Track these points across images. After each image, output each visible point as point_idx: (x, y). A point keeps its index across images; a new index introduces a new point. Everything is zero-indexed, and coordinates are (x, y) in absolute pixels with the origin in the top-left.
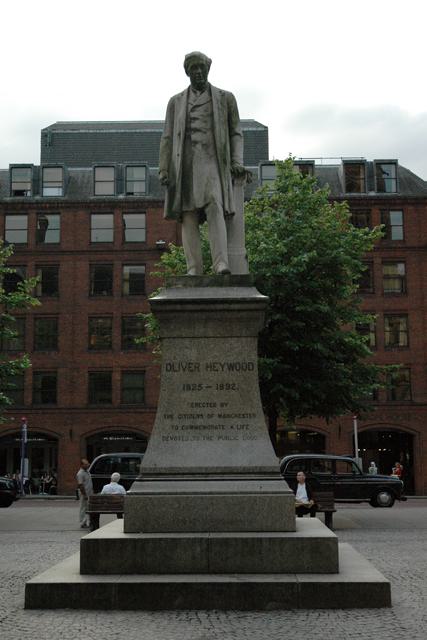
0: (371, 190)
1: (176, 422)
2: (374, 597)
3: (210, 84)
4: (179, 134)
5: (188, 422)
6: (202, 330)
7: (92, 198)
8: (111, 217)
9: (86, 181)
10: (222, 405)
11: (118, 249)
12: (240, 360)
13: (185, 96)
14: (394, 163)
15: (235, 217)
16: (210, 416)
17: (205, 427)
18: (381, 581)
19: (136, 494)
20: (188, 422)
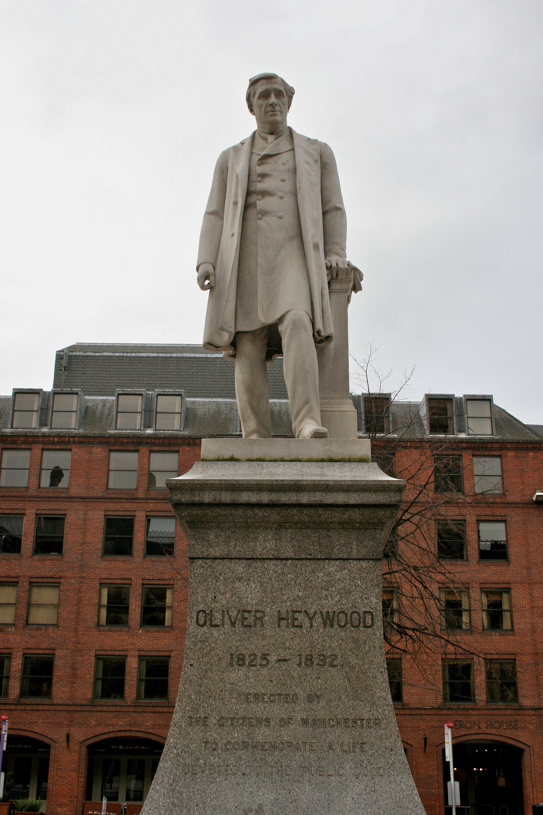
3: (290, 129)
4: (236, 203)
5: (238, 735)
6: (270, 545)
7: (112, 432)
9: (106, 412)
10: (310, 699)
11: (141, 496)
12: (347, 605)
13: (247, 147)
14: (488, 399)
16: (285, 722)
17: (273, 747)
20: (238, 735)
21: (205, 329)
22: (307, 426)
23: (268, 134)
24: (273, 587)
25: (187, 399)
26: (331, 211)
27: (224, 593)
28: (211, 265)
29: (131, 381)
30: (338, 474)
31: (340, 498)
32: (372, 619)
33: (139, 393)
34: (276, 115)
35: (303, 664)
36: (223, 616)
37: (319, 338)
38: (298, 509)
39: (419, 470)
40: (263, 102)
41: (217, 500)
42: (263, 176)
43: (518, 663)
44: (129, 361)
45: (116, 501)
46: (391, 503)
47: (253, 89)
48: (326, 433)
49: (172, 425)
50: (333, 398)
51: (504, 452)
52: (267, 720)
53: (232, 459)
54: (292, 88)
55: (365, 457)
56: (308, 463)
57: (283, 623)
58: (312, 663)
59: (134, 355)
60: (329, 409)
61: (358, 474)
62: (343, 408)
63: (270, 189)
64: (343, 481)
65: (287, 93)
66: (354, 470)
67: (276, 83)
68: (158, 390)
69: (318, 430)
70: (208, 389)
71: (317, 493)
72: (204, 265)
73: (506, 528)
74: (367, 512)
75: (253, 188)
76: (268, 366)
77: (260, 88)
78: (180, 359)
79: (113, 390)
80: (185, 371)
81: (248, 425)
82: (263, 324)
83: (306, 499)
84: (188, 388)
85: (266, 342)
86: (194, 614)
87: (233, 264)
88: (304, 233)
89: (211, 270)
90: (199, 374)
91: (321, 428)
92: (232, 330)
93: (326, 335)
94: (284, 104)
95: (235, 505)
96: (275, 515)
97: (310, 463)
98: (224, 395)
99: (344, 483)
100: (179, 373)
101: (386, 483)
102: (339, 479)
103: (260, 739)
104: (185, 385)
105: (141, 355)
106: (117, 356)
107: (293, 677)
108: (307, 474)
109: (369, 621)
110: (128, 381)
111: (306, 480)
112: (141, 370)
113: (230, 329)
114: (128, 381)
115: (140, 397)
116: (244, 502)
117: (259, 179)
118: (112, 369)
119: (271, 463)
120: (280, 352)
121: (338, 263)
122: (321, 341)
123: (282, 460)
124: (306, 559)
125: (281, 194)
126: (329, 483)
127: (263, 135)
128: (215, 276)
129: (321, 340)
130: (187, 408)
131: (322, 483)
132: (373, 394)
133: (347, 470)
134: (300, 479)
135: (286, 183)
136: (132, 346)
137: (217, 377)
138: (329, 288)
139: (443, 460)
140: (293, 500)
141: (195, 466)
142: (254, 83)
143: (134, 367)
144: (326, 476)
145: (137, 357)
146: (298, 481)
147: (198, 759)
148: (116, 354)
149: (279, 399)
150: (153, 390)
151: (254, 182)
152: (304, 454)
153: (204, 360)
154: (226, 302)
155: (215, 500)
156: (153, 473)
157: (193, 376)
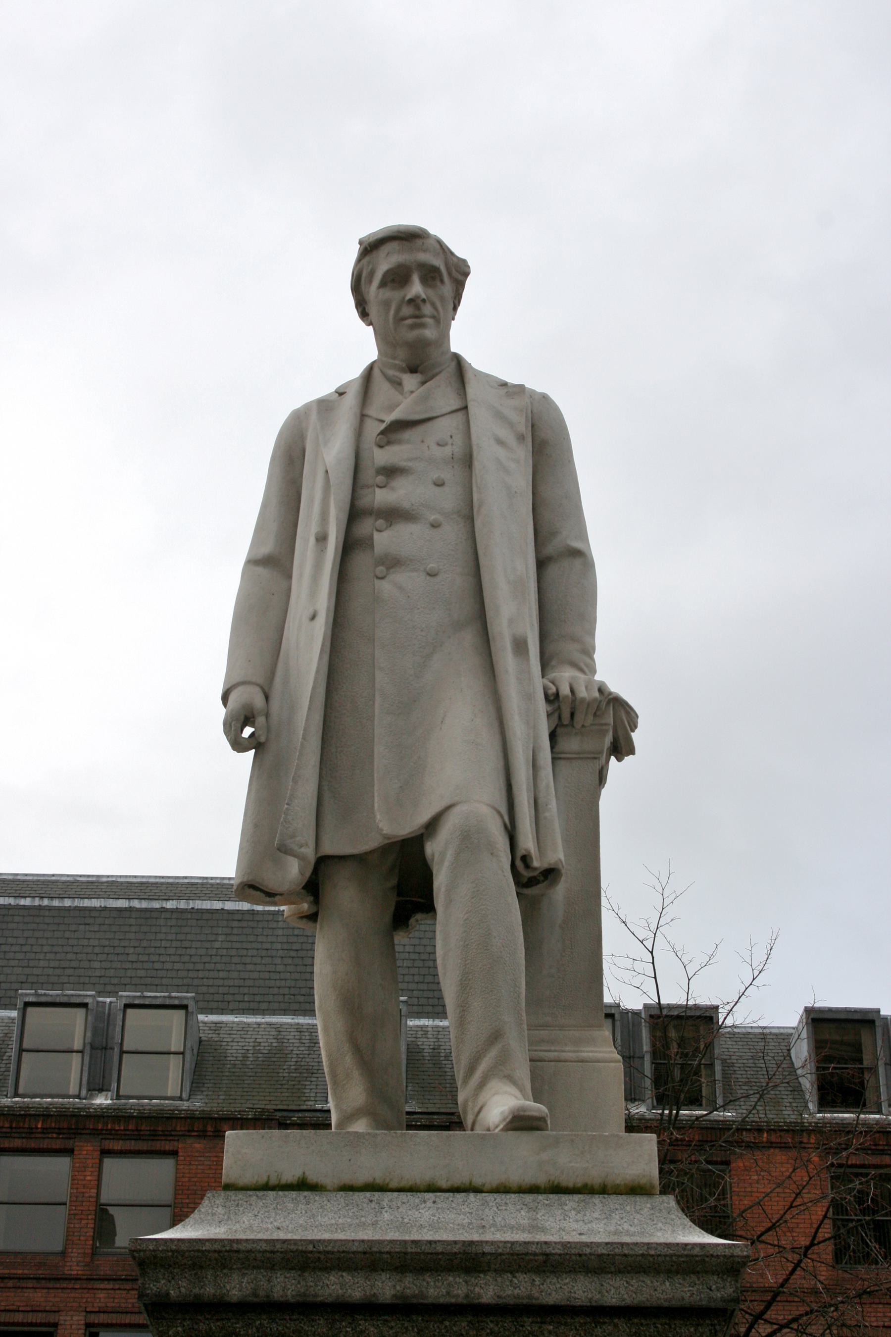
3: (458, 360)
4: (322, 539)
8: (63, 1164)
13: (351, 401)
21: (241, 849)
22: (496, 1098)
23: (403, 371)
25: (201, 1017)
26: (559, 559)
28: (257, 690)
29: (58, 972)
30: (575, 1226)
31: (581, 1290)
33: (78, 1001)
34: (423, 326)
37: (526, 874)
38: (470, 1318)
39: (791, 1207)
40: (395, 295)
41: (262, 1293)
42: (391, 472)
44: (57, 920)
45: (10, 1284)
46: (713, 1305)
47: (369, 263)
48: (542, 1119)
49: (161, 1084)
50: (562, 1027)
53: (303, 1185)
54: (464, 261)
55: (643, 1181)
56: (499, 1198)
59: (67, 903)
60: (552, 1055)
61: (626, 1226)
62: (588, 1052)
63: (406, 505)
64: (587, 1245)
65: (450, 274)
66: (616, 1217)
67: (425, 251)
68: (127, 995)
69: (523, 1109)
70: (255, 990)
71: (521, 1276)
72: (240, 689)
75: (365, 501)
76: (396, 942)
77: (385, 262)
78: (185, 916)
79: (12, 993)
80: (198, 944)
81: (344, 1097)
82: (386, 837)
83: (491, 1293)
84: (204, 989)
85: (394, 881)
87: (314, 688)
88: (489, 614)
89: (259, 701)
90: (233, 952)
91: (531, 1104)
92: (309, 852)
93: (546, 866)
94: (442, 298)
95: (306, 1308)
97: (503, 1196)
98: (294, 1006)
99: (588, 1251)
100: (183, 951)
101: (697, 1251)
102: (576, 1238)
104: (196, 982)
105: (87, 903)
106: (24, 907)
108: (494, 1225)
110: (51, 971)
111: (492, 1243)
112: (85, 942)
113: (303, 850)
114: (51, 971)
115: (81, 1012)
116: (330, 1300)
117: (381, 479)
118: (10, 940)
119: (403, 1196)
120: (428, 907)
121: (575, 686)
122: (532, 882)
123: (432, 1188)
125: (432, 517)
126: (549, 1250)
127: (391, 372)
128: (267, 715)
129: (532, 880)
130: (200, 1041)
131: (533, 1248)
132: (670, 1007)
133: (596, 1215)
134: (476, 1237)
135: (446, 489)
136: (64, 882)
137: (278, 961)
138: (552, 747)
139: (851, 1181)
140: (458, 1296)
141: (206, 1202)
142: (370, 248)
143: (67, 935)
144: (543, 1230)
145: (77, 908)
146: (471, 1243)
148: (22, 902)
149: (433, 1018)
150: (113, 994)
151: (368, 487)
152: (487, 1172)
153: (247, 917)
154: (295, 781)
155: (255, 1295)
156: (108, 1208)
157: (218, 959)
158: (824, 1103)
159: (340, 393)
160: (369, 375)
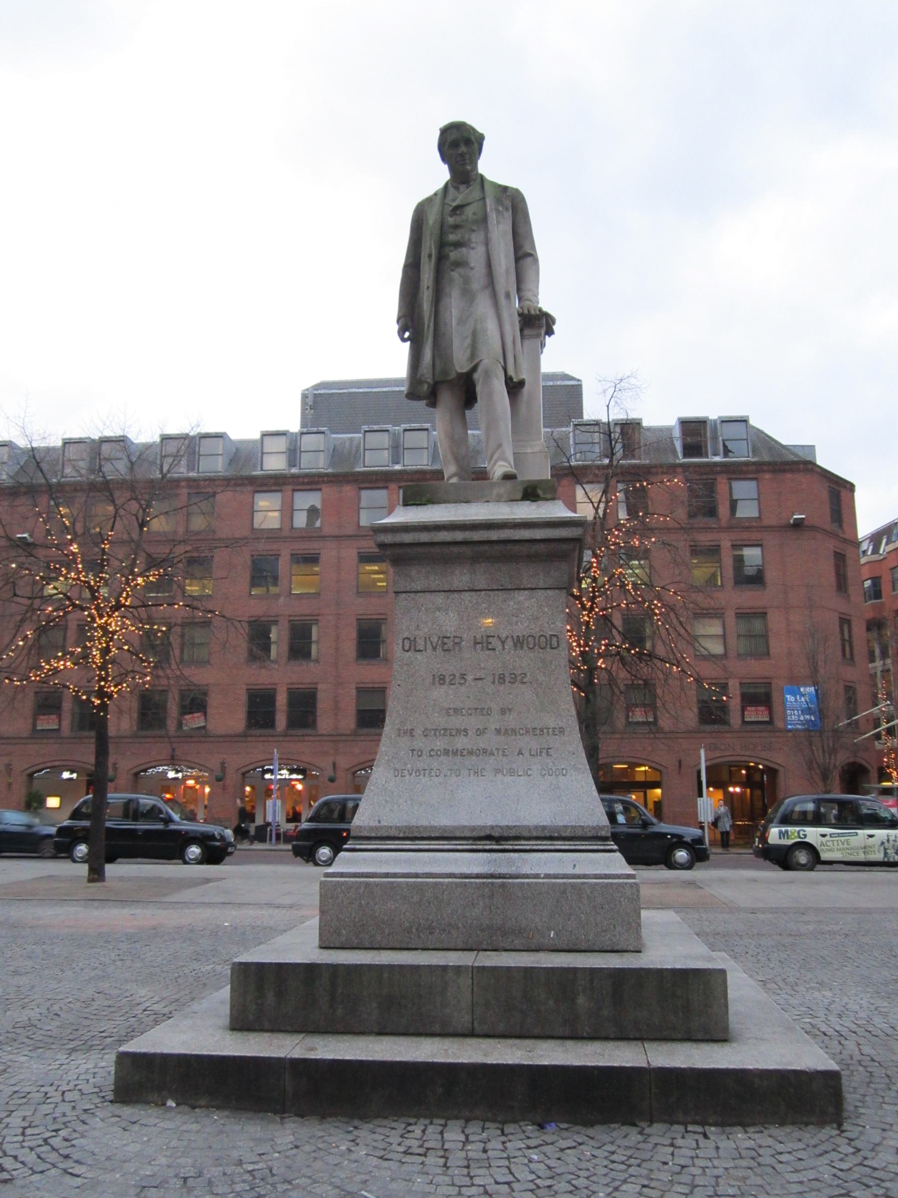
0: (715, 454)
1: (419, 743)
2: (805, 1100)
3: (482, 177)
8: (384, 493)
10: (503, 712)
14: (744, 421)
15: (526, 389)
16: (480, 732)
17: (471, 753)
18: (821, 1067)
19: (342, 875)
20: (440, 744)
24: (469, 615)
27: (426, 623)
32: (558, 642)
35: (497, 682)
36: (426, 643)
43: (773, 686)
51: (761, 475)
52: (465, 730)
57: (479, 646)
58: (505, 681)
73: (762, 552)
74: (553, 546)
86: (400, 642)
92: (430, 380)
96: (467, 551)
103: (459, 746)
107: (488, 694)
109: (555, 643)
115: (386, 433)
117: (451, 230)
124: (498, 590)
147: (406, 764)
158: (686, 454)
159: (435, 194)
160: (446, 187)
